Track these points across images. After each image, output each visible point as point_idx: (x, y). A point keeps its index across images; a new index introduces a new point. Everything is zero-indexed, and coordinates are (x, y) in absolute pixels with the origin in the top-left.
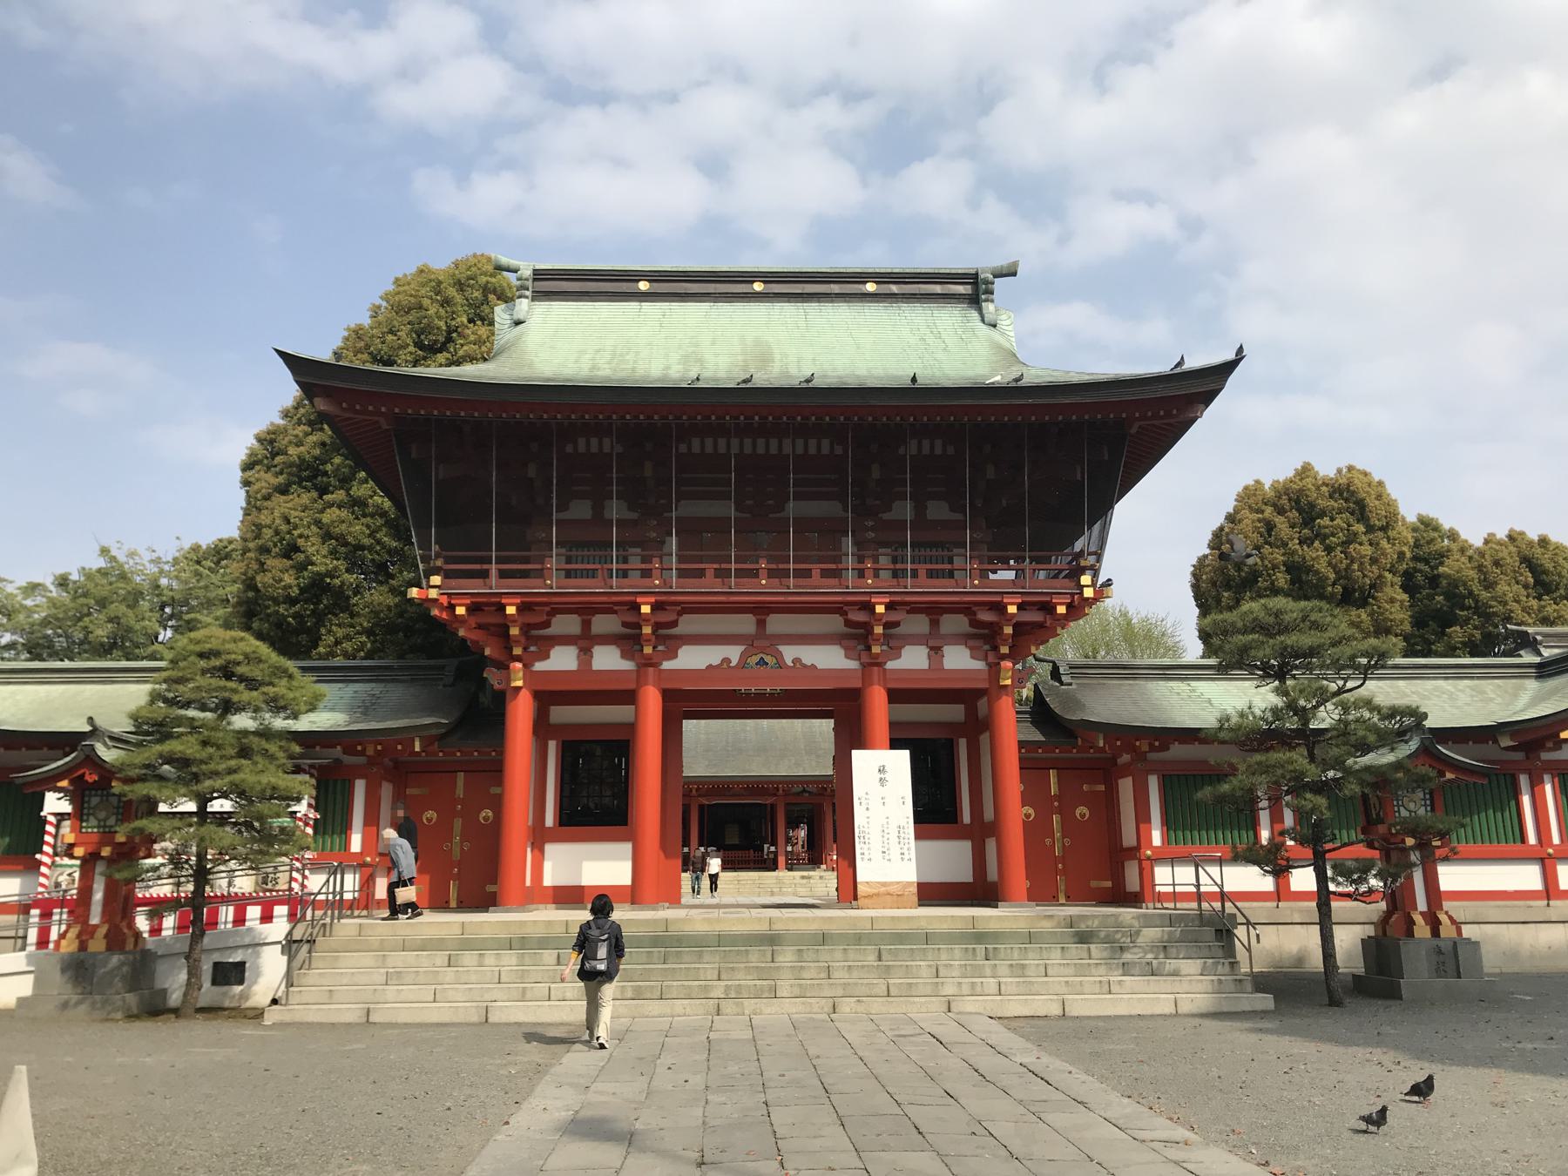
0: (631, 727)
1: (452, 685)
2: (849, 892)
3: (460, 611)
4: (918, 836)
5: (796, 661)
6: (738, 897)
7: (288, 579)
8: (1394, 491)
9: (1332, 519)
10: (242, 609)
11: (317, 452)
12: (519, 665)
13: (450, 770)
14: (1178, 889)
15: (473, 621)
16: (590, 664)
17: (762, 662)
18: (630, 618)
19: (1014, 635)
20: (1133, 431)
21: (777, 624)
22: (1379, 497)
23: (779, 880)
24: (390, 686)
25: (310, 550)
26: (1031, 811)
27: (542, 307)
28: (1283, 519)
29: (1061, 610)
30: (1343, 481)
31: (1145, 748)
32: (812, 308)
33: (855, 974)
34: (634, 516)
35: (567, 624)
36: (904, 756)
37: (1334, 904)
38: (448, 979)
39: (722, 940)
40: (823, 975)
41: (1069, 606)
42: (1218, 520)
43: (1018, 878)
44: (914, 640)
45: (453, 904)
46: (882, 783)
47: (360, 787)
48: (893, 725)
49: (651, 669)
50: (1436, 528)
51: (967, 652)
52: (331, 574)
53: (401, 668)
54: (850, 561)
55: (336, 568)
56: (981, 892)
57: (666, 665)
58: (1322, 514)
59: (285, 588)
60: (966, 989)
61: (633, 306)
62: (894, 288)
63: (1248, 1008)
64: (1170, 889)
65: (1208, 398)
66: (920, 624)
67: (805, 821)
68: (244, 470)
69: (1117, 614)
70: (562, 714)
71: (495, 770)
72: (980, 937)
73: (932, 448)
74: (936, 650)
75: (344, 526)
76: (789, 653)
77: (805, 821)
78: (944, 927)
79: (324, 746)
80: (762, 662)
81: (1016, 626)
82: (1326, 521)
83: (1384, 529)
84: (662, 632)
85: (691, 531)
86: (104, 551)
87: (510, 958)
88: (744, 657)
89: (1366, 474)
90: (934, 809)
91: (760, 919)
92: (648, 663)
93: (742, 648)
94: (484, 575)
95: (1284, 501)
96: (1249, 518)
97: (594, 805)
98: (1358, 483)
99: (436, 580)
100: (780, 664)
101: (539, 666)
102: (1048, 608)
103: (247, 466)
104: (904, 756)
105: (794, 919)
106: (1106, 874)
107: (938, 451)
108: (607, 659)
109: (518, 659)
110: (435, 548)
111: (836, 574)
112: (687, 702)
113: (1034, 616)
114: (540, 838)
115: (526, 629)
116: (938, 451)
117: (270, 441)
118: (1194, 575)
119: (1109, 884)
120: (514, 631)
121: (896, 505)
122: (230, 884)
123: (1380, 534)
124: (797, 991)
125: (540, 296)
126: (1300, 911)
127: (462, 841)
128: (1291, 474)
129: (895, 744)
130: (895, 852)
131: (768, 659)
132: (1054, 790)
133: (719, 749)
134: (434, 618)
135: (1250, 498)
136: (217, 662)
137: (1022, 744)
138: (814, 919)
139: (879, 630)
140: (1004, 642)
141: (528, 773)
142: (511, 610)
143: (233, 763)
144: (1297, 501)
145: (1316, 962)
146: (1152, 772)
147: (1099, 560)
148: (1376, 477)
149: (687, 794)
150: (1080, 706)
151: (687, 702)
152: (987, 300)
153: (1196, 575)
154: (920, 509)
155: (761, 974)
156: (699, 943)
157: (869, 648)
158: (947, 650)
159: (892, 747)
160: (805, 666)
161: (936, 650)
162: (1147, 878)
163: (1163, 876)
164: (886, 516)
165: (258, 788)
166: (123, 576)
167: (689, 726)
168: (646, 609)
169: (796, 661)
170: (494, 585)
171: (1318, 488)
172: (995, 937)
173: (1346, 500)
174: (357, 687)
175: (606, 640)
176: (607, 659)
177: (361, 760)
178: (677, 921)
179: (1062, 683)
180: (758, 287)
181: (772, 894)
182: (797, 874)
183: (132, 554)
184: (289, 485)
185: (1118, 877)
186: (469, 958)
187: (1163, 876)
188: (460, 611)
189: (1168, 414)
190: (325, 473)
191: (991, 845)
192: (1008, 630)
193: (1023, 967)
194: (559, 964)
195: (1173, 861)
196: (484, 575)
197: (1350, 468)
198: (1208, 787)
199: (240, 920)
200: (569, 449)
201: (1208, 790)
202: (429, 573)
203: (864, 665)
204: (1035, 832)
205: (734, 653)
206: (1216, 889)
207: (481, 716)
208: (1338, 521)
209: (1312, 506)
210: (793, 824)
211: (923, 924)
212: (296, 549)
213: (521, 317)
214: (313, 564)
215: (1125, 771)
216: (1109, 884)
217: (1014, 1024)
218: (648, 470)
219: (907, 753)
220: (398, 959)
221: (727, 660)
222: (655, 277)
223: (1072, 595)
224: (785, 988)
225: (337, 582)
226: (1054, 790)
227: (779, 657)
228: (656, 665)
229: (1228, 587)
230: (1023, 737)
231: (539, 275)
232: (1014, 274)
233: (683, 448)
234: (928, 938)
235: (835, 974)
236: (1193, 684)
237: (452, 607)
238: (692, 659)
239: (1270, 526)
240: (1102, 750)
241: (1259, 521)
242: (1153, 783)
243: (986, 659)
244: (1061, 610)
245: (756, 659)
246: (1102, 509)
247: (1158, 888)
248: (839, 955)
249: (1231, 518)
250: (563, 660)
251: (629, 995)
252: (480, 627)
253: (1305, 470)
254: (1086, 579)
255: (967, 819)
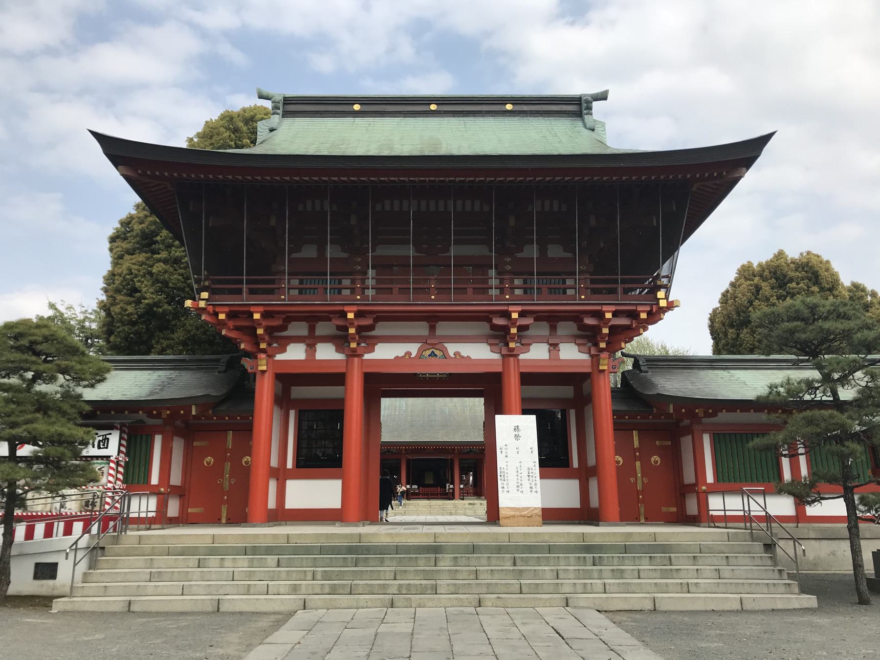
0: (342, 401)
1: (225, 372)
2: (494, 516)
3: (222, 316)
4: (542, 476)
5: (457, 354)
6: (416, 517)
7: (130, 309)
8: (836, 266)
9: (798, 284)
10: (105, 329)
11: (153, 227)
12: (263, 356)
13: (223, 429)
14: (728, 513)
15: (231, 324)
16: (314, 356)
17: (433, 354)
18: (341, 323)
19: (609, 335)
20: (694, 189)
21: (443, 328)
22: (827, 270)
23: (455, 506)
24: (184, 373)
25: (144, 290)
26: (620, 459)
27: (288, 121)
28: (766, 284)
29: (643, 316)
30: (805, 260)
31: (701, 414)
32: (470, 121)
33: (496, 576)
34: (345, 255)
35: (299, 329)
36: (532, 419)
37: (862, 526)
38: (195, 578)
39: (398, 549)
40: (473, 576)
41: (649, 313)
42: (725, 286)
43: (613, 506)
44: (539, 340)
45: (224, 521)
46: (517, 439)
47: (158, 441)
48: (524, 400)
49: (356, 359)
50: (863, 290)
51: (576, 348)
52: (157, 304)
53: (190, 361)
54: (494, 282)
55: (160, 301)
56: (585, 515)
57: (367, 356)
58: (791, 280)
59: (128, 315)
60: (579, 589)
61: (350, 120)
62: (525, 108)
63: (797, 606)
64: (722, 513)
65: (748, 163)
66: (543, 329)
67: (466, 469)
68: (110, 242)
69: (660, 348)
70: (299, 392)
71: (246, 429)
72: (588, 549)
73: (551, 206)
74: (554, 346)
75: (166, 276)
76: (452, 348)
77: (466, 469)
78: (562, 541)
79: (130, 412)
80: (433, 354)
81: (612, 328)
82: (794, 285)
83: (831, 290)
84: (364, 334)
85: (382, 266)
86: (52, 306)
87: (243, 560)
88: (420, 351)
89: (818, 256)
90: (553, 457)
91: (427, 534)
92: (353, 354)
93: (419, 345)
94: (239, 292)
95: (766, 273)
96: (746, 284)
97: (319, 453)
98: (814, 261)
99: (205, 295)
100: (445, 356)
101: (279, 357)
102: (633, 315)
103: (113, 240)
104: (532, 419)
105: (453, 534)
106: (678, 503)
107: (556, 209)
108: (326, 353)
109: (264, 351)
110: (204, 272)
111: (485, 290)
112: (384, 384)
113: (623, 321)
114: (281, 475)
115: (269, 330)
116: (556, 209)
117: (126, 223)
118: (710, 319)
119: (674, 509)
120: (260, 331)
121: (526, 248)
122: (62, 506)
123: (828, 293)
124: (452, 589)
125: (286, 114)
126: (814, 530)
127: (230, 478)
128: (771, 256)
129: (525, 412)
130: (526, 484)
131: (437, 352)
132: (636, 444)
133: (406, 419)
134: (225, 338)
135: (746, 272)
136: (24, 342)
137: (615, 412)
138: (467, 534)
139: (514, 331)
140: (603, 340)
141: (275, 436)
142: (257, 316)
143: (30, 416)
144: (775, 273)
145: (847, 567)
146: (705, 431)
147: (670, 281)
148: (825, 258)
149: (382, 446)
150: (652, 385)
151: (384, 384)
152: (587, 114)
153: (712, 320)
154: (543, 251)
155: (427, 575)
156: (381, 551)
157: (507, 345)
158: (562, 346)
159: (523, 414)
160: (463, 357)
161: (554, 346)
162: (703, 505)
163: (715, 504)
164: (519, 255)
165: (47, 434)
166: (63, 321)
167: (386, 403)
168: (351, 316)
169: (457, 354)
170: (244, 299)
171: (788, 265)
172: (599, 548)
173: (806, 272)
174: (161, 373)
175: (325, 339)
176: (326, 353)
177: (158, 422)
178: (367, 535)
179: (641, 371)
180: (433, 107)
181: (451, 514)
182: (466, 502)
183: (69, 308)
184: (134, 249)
185: (682, 506)
186: (214, 560)
187: (715, 504)
188: (222, 316)
189: (720, 175)
190: (157, 242)
191: (593, 484)
192: (606, 331)
193: (622, 571)
194: (278, 566)
195: (723, 492)
196: (239, 292)
197: (808, 253)
198: (750, 441)
199: (29, 534)
200: (301, 208)
201: (757, 441)
202: (200, 291)
203: (503, 356)
204: (624, 473)
205: (413, 348)
206: (764, 514)
207: (241, 389)
208: (801, 285)
209: (785, 276)
210: (464, 471)
211: (547, 538)
212: (136, 290)
213: (274, 127)
214: (145, 298)
215: (688, 431)
216: (674, 509)
217: (618, 618)
218: (353, 221)
219: (534, 416)
220: (163, 562)
221: (409, 353)
222: (363, 101)
223: (651, 305)
224: (443, 583)
225: (160, 310)
226: (636, 444)
227: (444, 352)
228: (361, 356)
229: (732, 326)
230: (615, 408)
231: (287, 101)
232: (605, 99)
233: (378, 207)
234: (550, 549)
235: (481, 576)
236: (732, 372)
237: (216, 314)
238: (385, 353)
239: (758, 289)
240: (670, 416)
241: (751, 285)
242: (706, 440)
243: (589, 353)
244: (643, 316)
245: (428, 352)
246: (671, 249)
247: (711, 513)
248: (484, 561)
249: (733, 285)
250: (295, 353)
251: (327, 591)
252: (237, 328)
253: (780, 254)
254: (661, 294)
255: (575, 464)
